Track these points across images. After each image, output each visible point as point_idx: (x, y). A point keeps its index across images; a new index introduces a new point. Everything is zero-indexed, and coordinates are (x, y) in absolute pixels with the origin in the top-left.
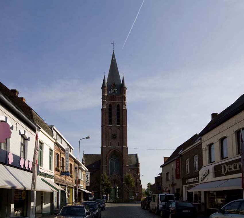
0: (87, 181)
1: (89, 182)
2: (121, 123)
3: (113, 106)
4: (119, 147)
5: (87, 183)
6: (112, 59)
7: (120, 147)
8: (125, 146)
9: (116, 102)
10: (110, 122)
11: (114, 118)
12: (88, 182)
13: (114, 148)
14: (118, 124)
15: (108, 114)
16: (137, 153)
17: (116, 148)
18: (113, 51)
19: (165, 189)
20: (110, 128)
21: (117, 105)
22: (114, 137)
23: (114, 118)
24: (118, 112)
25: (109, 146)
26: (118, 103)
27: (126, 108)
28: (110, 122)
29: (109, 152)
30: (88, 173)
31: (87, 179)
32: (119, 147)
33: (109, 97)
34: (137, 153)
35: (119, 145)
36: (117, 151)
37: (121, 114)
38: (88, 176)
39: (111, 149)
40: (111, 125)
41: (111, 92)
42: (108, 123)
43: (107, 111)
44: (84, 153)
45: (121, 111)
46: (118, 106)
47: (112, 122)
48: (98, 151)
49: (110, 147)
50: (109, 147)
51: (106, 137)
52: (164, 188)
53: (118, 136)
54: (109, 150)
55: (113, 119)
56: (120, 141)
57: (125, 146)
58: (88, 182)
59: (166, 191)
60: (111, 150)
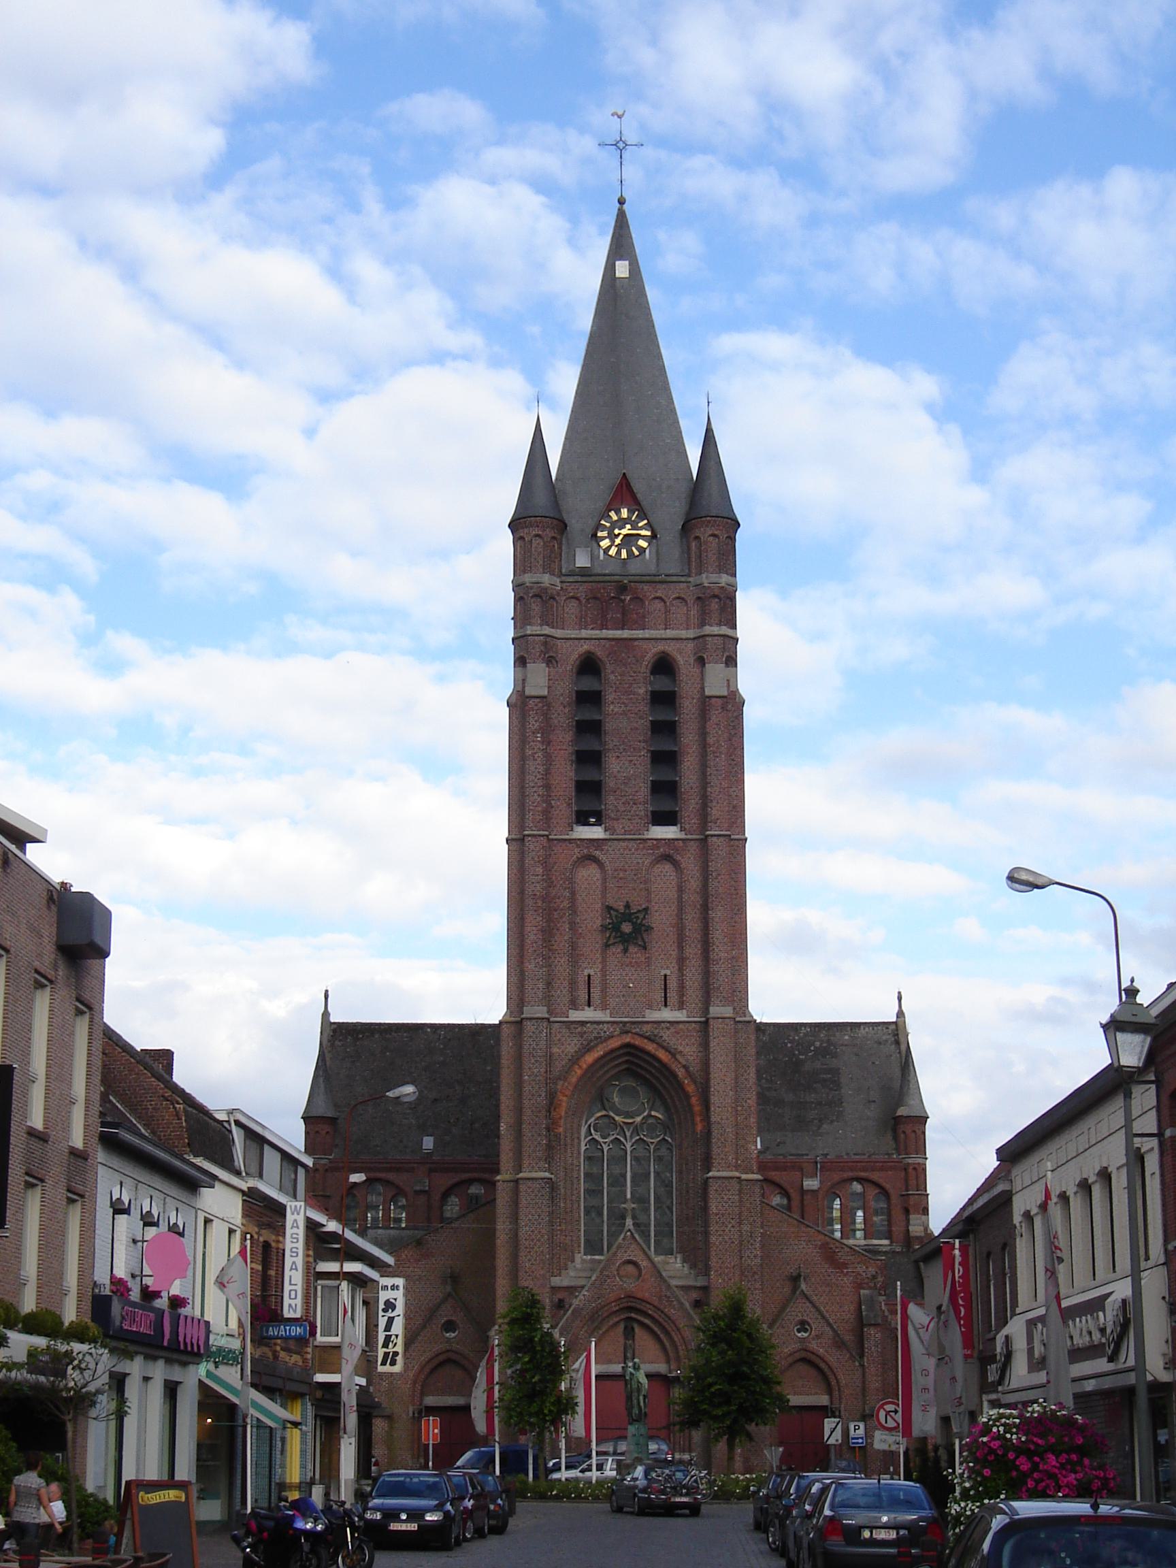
0: (385, 1345)
1: (399, 1348)
2: (689, 806)
3: (612, 674)
4: (667, 1015)
5: (387, 1354)
6: (610, 268)
7: (680, 1016)
8: (727, 1011)
9: (647, 634)
10: (589, 800)
11: (627, 769)
12: (390, 1349)
13: (625, 1028)
14: (664, 818)
15: (564, 741)
16: (901, 1014)
17: (646, 1028)
18: (621, 202)
19: (882, 1414)
20: (590, 854)
21: (649, 658)
22: (627, 929)
23: (627, 769)
24: (662, 716)
25: (574, 1005)
26: (661, 647)
27: (731, 682)
28: (589, 800)
29: (575, 1060)
30: (394, 1287)
31: (388, 1327)
32: (667, 1015)
33: (582, 595)
34: (901, 1014)
35: (673, 996)
36: (650, 1047)
37: (688, 737)
38: (393, 1307)
39: (588, 1035)
40: (596, 832)
41: (593, 558)
42: (563, 808)
43: (563, 716)
44: (326, 1014)
45: (688, 707)
46: (664, 666)
47: (610, 802)
48: (465, 986)
49: (588, 1014)
50: (575, 1016)
51: (548, 933)
52: (882, 1407)
53: (661, 919)
54: (571, 1046)
55: (610, 783)
56: (681, 961)
57: (727, 1011)
58: (390, 1349)
59: (891, 1424)
60: (600, 1040)
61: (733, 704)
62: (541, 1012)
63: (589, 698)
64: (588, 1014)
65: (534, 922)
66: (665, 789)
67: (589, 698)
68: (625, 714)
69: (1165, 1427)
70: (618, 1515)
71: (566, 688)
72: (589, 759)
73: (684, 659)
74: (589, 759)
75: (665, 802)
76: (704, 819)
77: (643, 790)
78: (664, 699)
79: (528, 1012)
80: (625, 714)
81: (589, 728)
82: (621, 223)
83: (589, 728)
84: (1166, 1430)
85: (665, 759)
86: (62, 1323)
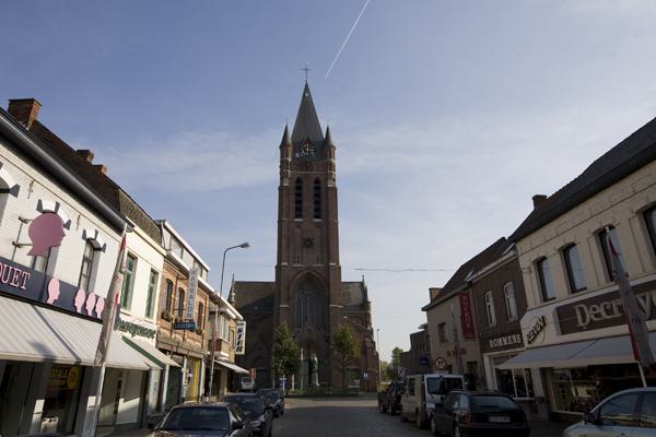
10: (299, 212)
11: (308, 205)
14: (317, 217)
15: (293, 198)
20: (299, 225)
22: (308, 243)
23: (308, 205)
25: (294, 262)
28: (299, 212)
29: (294, 276)
37: (323, 203)
40: (300, 220)
42: (293, 214)
43: (293, 191)
46: (317, 181)
51: (288, 245)
54: (293, 273)
56: (322, 252)
61: (335, 189)
62: (286, 264)
63: (299, 188)
64: (299, 265)
65: (284, 242)
66: (317, 210)
67: (299, 188)
68: (308, 191)
69: (93, 395)
70: (82, 259)
71: (294, 185)
72: (299, 202)
73: (321, 179)
74: (299, 202)
75: (318, 213)
76: (328, 216)
77: (312, 210)
78: (317, 188)
79: (283, 264)
80: (308, 191)
81: (299, 195)
82: (307, 85)
83: (299, 195)
84: (94, 398)
85: (317, 203)
86: (369, 350)
